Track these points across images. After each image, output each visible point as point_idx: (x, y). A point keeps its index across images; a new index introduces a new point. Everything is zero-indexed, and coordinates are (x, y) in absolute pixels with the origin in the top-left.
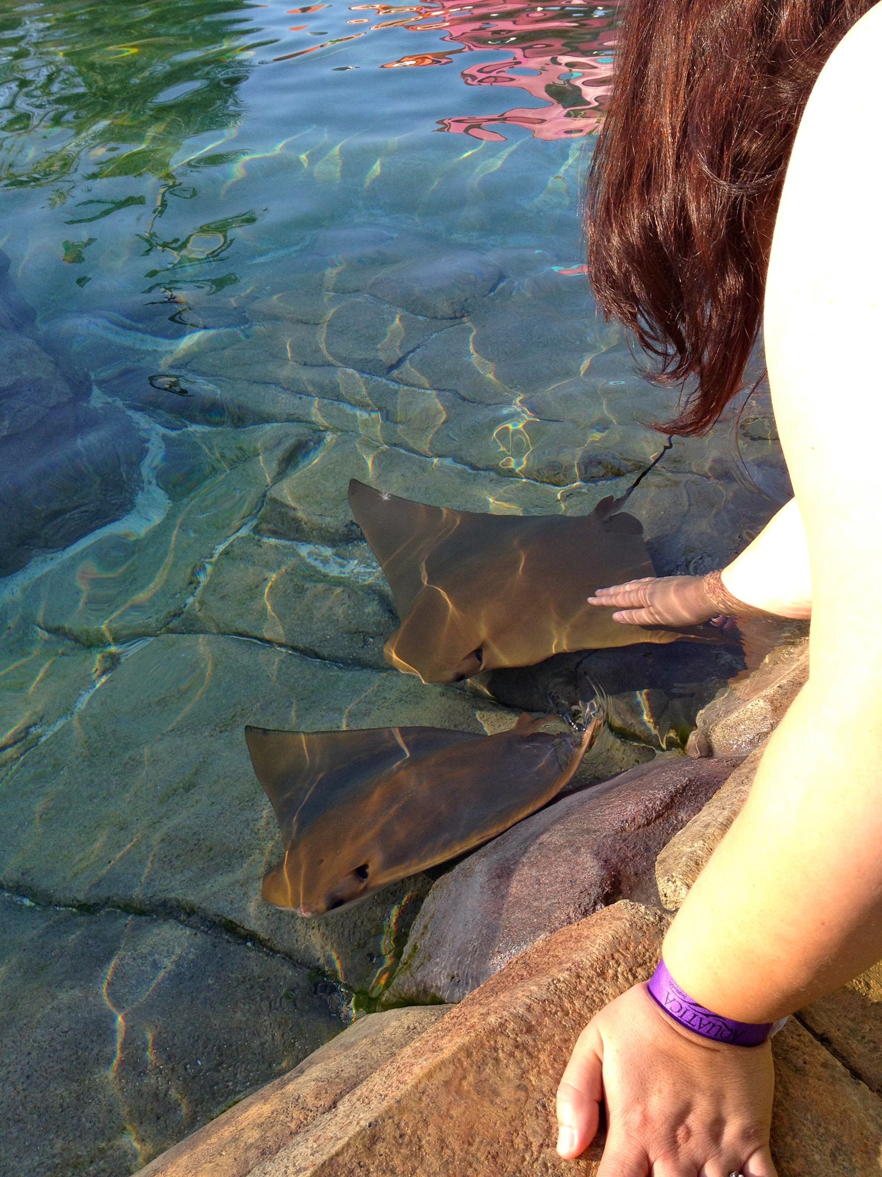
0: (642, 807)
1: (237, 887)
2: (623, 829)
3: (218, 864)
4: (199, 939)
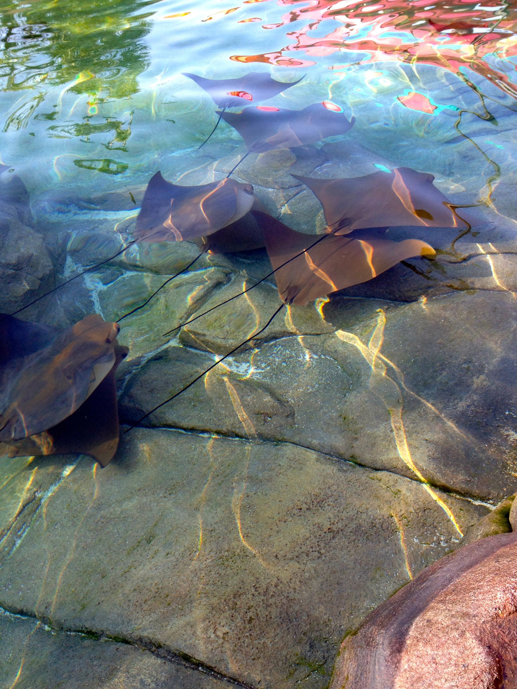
0: (509, 595)
1: (189, 628)
2: (497, 615)
3: (173, 609)
4: (168, 666)
